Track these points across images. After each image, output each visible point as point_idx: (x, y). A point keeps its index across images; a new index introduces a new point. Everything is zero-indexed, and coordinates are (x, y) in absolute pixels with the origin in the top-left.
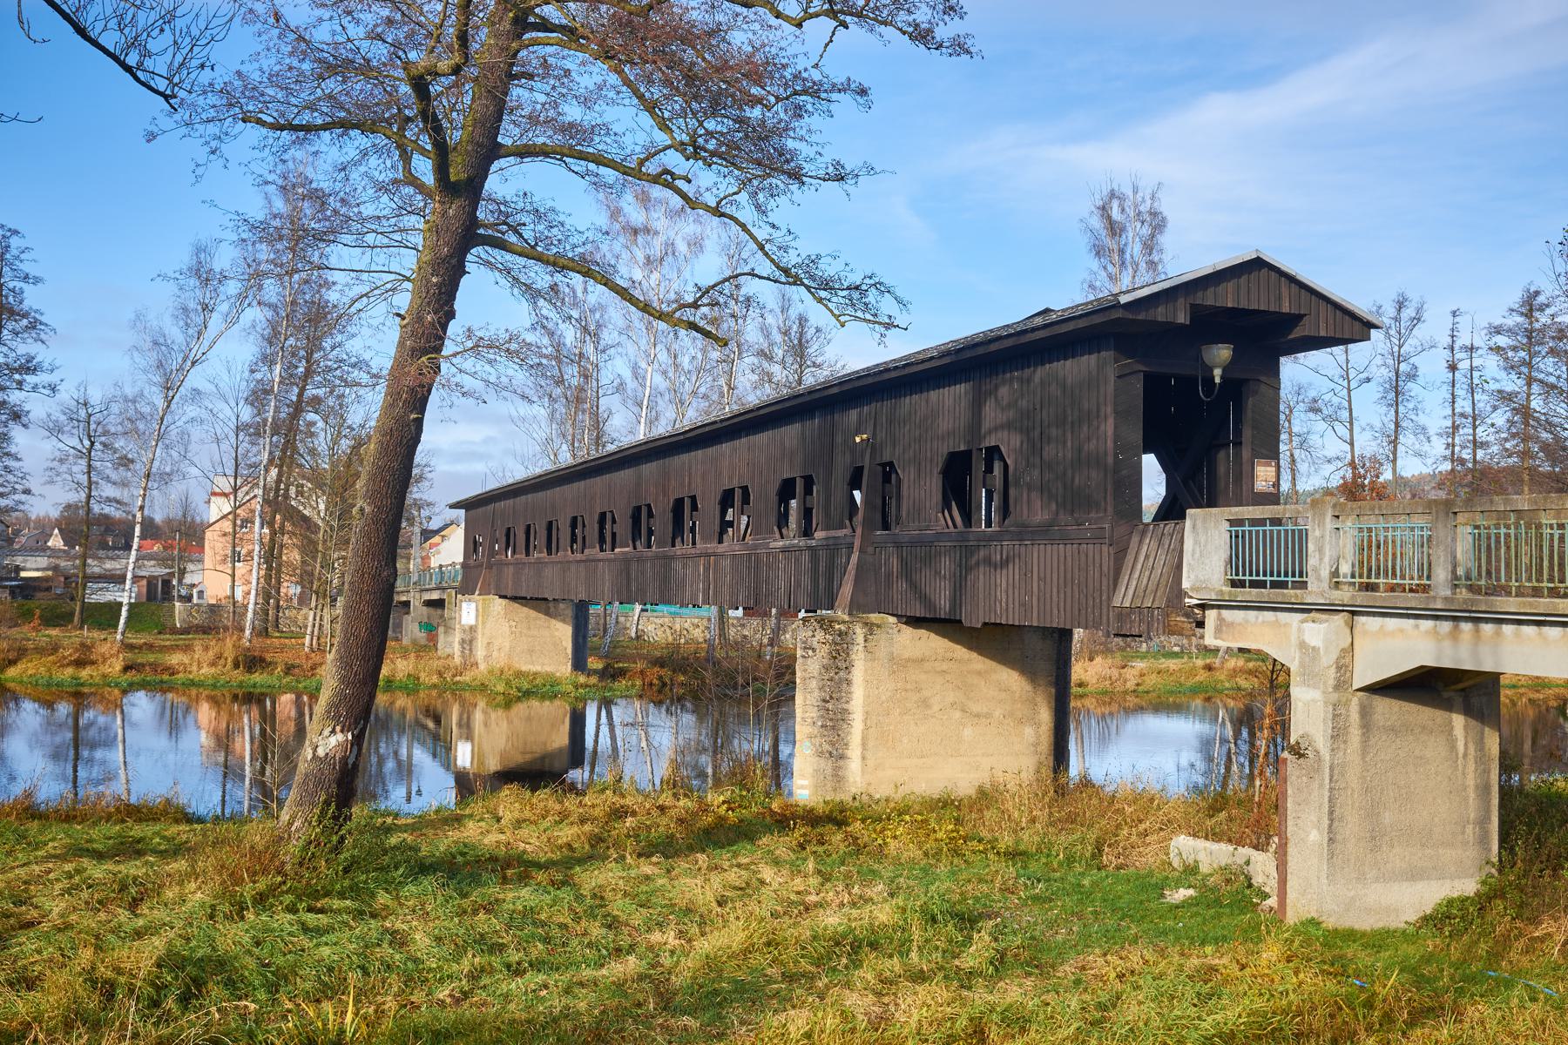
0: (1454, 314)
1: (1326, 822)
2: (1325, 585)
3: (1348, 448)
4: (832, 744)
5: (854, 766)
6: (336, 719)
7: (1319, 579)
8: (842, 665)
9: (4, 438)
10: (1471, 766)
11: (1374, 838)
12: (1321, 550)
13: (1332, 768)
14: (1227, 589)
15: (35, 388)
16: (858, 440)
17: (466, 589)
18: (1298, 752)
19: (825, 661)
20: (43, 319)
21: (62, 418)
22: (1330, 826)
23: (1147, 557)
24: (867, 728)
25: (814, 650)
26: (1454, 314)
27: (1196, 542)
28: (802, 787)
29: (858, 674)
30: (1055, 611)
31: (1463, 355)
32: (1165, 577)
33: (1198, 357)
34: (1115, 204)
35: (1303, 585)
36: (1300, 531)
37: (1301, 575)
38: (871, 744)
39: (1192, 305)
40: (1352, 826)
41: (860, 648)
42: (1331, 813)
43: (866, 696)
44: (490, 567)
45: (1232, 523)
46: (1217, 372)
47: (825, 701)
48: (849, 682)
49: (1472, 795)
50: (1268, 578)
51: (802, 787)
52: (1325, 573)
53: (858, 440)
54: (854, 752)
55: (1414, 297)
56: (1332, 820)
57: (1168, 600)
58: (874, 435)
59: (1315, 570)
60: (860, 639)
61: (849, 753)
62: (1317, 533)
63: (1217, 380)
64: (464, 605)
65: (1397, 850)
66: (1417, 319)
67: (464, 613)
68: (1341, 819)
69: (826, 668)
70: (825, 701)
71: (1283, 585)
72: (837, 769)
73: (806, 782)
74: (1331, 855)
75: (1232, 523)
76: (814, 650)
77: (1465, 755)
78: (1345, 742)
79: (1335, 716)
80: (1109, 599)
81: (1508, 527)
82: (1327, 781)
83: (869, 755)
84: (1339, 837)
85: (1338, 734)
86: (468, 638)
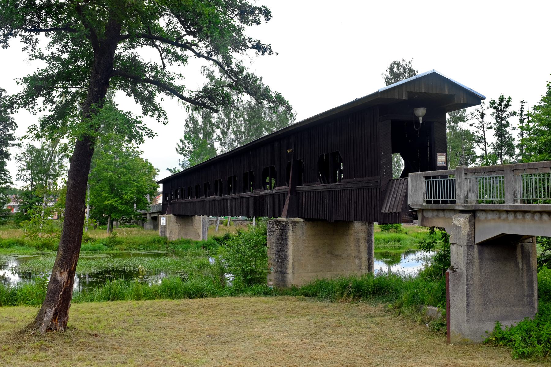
0: (522, 102)
1: (465, 298)
2: (463, 201)
3: (484, 152)
4: (281, 268)
5: (290, 276)
6: (62, 266)
7: (460, 199)
8: (284, 238)
9: (4, 164)
10: (525, 274)
11: (485, 304)
12: (460, 188)
13: (467, 276)
14: (425, 204)
15: (13, 145)
16: (288, 152)
17: (162, 212)
18: (453, 269)
19: (278, 237)
20: (15, 121)
21: (22, 155)
22: (467, 300)
23: (394, 192)
24: (294, 262)
25: (273, 232)
26: (522, 102)
27: (413, 186)
28: (270, 285)
29: (290, 241)
30: (360, 215)
31: (525, 117)
32: (401, 200)
33: (413, 114)
34: (396, 67)
35: (454, 202)
36: (452, 180)
37: (453, 198)
38: (296, 267)
39: (408, 92)
40: (476, 299)
41: (291, 231)
42: (467, 294)
43: (294, 250)
44: (171, 204)
45: (427, 178)
46: (421, 119)
47: (278, 252)
48: (287, 244)
49: (526, 285)
50: (441, 199)
51: (270, 285)
52: (462, 197)
53: (288, 152)
54: (290, 271)
55: (506, 97)
56: (468, 297)
57: (402, 209)
58: (295, 150)
59: (459, 196)
60: (291, 228)
61: (288, 271)
62: (459, 181)
63: (421, 122)
64: (162, 218)
65: (495, 308)
66: (508, 105)
67: (162, 222)
68: (472, 297)
69: (278, 239)
70: (278, 252)
71: (446, 202)
72: (284, 277)
73: (272, 283)
74: (468, 311)
75: (427, 178)
76: (273, 232)
77: (522, 269)
78: (472, 265)
79: (468, 255)
80: (380, 210)
81: (539, 176)
82: (465, 281)
83: (295, 272)
84: (471, 304)
85: (469, 263)
86: (163, 230)
